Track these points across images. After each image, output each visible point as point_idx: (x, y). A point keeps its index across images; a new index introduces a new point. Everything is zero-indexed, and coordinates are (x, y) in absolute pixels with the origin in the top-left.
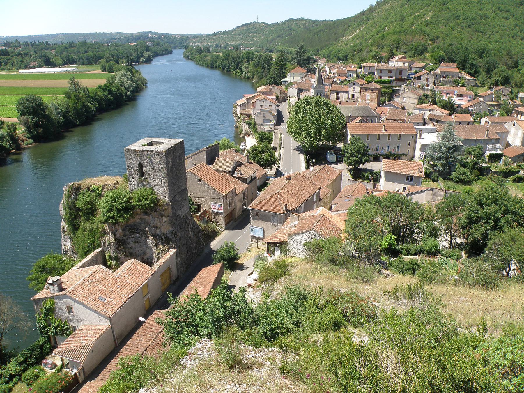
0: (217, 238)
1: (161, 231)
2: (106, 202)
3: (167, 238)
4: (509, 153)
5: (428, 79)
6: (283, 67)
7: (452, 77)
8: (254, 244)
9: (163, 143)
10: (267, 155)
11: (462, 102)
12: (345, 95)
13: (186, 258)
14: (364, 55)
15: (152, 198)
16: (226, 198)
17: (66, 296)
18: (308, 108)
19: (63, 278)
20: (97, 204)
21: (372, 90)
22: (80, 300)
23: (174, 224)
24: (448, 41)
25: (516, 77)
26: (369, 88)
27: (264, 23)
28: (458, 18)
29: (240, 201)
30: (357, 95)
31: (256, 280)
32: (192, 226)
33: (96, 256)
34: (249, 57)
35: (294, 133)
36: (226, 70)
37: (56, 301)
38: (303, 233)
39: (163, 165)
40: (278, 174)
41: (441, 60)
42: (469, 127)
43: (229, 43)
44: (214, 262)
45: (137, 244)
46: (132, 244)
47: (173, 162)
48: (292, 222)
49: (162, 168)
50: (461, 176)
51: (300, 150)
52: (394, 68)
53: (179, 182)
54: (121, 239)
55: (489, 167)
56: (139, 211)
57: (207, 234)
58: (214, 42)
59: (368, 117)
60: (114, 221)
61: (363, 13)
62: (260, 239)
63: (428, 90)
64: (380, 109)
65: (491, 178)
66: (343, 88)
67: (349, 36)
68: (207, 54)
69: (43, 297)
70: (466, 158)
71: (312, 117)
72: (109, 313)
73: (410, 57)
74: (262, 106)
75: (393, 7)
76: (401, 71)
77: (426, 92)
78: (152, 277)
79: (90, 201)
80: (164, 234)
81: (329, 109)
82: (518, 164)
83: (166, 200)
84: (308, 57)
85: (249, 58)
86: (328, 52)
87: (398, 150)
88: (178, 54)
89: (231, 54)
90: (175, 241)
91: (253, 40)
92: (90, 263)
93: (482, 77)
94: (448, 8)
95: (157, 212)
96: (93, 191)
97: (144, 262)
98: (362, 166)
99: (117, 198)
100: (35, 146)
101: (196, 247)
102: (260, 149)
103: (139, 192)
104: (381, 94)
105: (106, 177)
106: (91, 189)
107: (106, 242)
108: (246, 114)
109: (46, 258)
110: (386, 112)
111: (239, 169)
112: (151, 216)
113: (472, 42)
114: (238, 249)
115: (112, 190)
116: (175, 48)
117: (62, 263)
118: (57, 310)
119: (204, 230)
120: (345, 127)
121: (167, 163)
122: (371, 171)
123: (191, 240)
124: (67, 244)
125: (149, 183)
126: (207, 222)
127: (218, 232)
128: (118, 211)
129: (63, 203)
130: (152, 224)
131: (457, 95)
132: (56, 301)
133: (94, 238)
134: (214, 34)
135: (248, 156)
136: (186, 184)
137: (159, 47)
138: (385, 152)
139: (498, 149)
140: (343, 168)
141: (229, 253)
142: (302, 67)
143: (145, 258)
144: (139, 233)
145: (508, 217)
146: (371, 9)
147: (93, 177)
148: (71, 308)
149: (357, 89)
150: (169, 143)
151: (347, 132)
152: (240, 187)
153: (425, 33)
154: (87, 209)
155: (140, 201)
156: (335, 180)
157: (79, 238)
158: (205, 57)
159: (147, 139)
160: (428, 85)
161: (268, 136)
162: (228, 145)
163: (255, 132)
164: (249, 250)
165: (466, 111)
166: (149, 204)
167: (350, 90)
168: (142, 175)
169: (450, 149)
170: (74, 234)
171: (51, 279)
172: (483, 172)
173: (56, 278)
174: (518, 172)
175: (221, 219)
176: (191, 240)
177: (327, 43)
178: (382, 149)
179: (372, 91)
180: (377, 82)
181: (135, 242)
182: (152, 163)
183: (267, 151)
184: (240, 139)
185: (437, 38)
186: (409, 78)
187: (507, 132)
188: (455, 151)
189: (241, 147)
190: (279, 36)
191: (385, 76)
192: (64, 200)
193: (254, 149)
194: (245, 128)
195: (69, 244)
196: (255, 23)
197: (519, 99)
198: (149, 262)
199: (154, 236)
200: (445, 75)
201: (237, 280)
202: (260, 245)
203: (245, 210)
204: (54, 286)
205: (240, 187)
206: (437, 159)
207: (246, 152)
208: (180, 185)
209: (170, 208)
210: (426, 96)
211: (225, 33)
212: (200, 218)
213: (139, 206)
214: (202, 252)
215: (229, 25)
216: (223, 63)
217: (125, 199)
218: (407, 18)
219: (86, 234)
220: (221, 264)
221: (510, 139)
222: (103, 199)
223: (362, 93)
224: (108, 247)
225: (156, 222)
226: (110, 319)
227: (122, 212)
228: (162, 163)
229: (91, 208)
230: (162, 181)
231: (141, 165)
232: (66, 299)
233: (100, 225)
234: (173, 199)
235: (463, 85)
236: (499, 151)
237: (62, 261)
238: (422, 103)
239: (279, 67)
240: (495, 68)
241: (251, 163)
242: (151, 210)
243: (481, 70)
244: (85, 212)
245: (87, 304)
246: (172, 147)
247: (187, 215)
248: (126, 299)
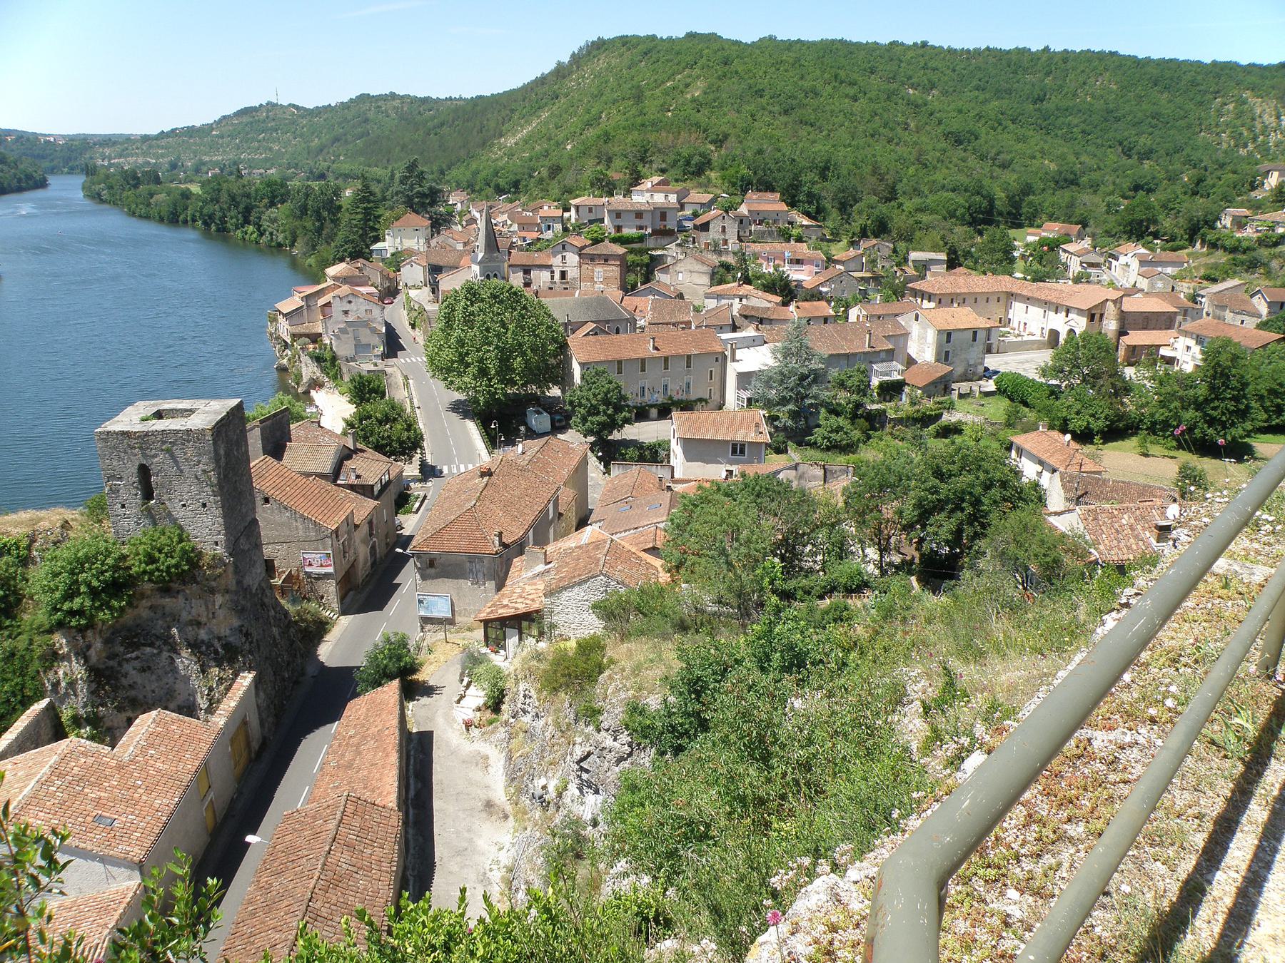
0: (327, 637)
1: (210, 632)
2: (56, 575)
3: (227, 646)
4: (918, 378)
5: (724, 228)
6: (369, 214)
7: (775, 221)
10: (399, 427)
11: (802, 276)
12: (545, 275)
13: (273, 693)
14: (569, 178)
15: (184, 552)
18: (475, 308)
21: (606, 259)
24: (752, 146)
25: (898, 221)
26: (600, 255)
27: (294, 106)
28: (760, 93)
29: (364, 541)
30: (572, 273)
31: (479, 709)
33: (36, 723)
34: (276, 194)
35: (445, 371)
36: (213, 228)
38: (580, 584)
39: (206, 464)
40: (428, 472)
41: (744, 186)
42: (829, 327)
43: (205, 158)
45: (147, 674)
47: (227, 455)
48: (531, 567)
49: (204, 472)
50: (833, 435)
51: (462, 409)
52: (646, 207)
55: (885, 411)
56: (148, 587)
58: (162, 156)
59: (607, 322)
60: (83, 622)
61: (541, 81)
63: (727, 252)
64: (631, 301)
65: (891, 434)
66: (538, 258)
67: (514, 135)
68: (153, 187)
70: (834, 397)
71: (488, 330)
72: (137, 853)
73: (677, 181)
74: (346, 312)
75: (609, 68)
76: (663, 214)
77: (723, 259)
78: (217, 745)
80: (219, 639)
81: (525, 308)
82: (937, 399)
83: (220, 550)
84: (430, 188)
85: (274, 197)
86: (468, 174)
87: (688, 392)
88: (67, 189)
89: (225, 186)
90: (250, 652)
91: (270, 149)
93: (834, 220)
94: (737, 72)
95: (198, 583)
98: (616, 436)
102: (378, 415)
104: (627, 268)
107: (58, 683)
108: (307, 335)
110: (644, 307)
111: (349, 464)
112: (180, 597)
113: (800, 145)
116: (52, 171)
120: (563, 347)
121: (217, 459)
122: (634, 443)
127: (327, 623)
128: (94, 593)
130: (185, 616)
131: (792, 262)
134: (162, 135)
137: (5, 168)
138: (660, 398)
139: (894, 372)
140: (575, 440)
141: (399, 658)
142: (417, 213)
144: (152, 645)
145: (995, 492)
146: (560, 72)
149: (572, 258)
150: (207, 413)
151: (568, 361)
152: (364, 508)
153: (698, 125)
155: (151, 560)
156: (577, 470)
158: (151, 195)
160: (726, 242)
161: (374, 385)
163: (335, 378)
165: (815, 295)
166: (177, 566)
167: (556, 261)
168: (148, 494)
169: (803, 378)
172: (875, 421)
174: (939, 416)
175: (330, 590)
177: (462, 153)
178: (653, 391)
179: (606, 260)
180: (614, 240)
181: (143, 670)
182: (176, 462)
183: (395, 419)
185: (726, 136)
186: (682, 229)
187: (906, 335)
188: (815, 381)
190: (336, 140)
191: (630, 227)
194: (309, 370)
196: (271, 106)
197: (910, 263)
199: (194, 646)
200: (759, 218)
201: (430, 719)
205: (364, 508)
206: (778, 404)
208: (244, 510)
209: (231, 569)
210: (727, 267)
211: (191, 131)
213: (151, 573)
214: (303, 674)
215: (203, 113)
216: (205, 211)
218: (648, 93)
221: (913, 350)
223: (584, 267)
225: (197, 609)
226: (140, 866)
228: (204, 459)
230: (204, 505)
231: (144, 471)
235: (799, 240)
236: (896, 377)
238: (720, 283)
239: (359, 216)
240: (856, 201)
243: (828, 206)
246: (222, 419)
248: (167, 811)
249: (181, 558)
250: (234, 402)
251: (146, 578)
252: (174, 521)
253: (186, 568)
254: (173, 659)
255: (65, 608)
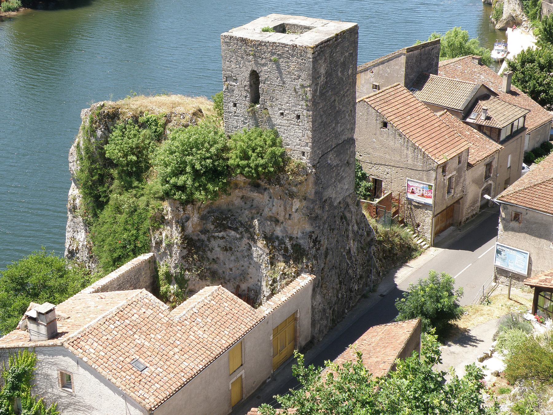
0: (412, 263)
1: (285, 230)
2: (172, 153)
3: (297, 248)
8: (502, 289)
9: (309, 28)
13: (334, 299)
15: (273, 154)
16: (444, 171)
17: (61, 350)
19: (61, 309)
20: (151, 155)
22: (90, 363)
23: (317, 217)
29: (476, 182)
31: (498, 375)
32: (356, 228)
33: (137, 270)
37: (40, 357)
39: (305, 79)
44: (399, 317)
45: (229, 254)
46: (218, 253)
47: (328, 74)
49: (302, 86)
53: (337, 123)
54: (195, 238)
57: (391, 250)
62: (518, 277)
69: (12, 345)
79: (137, 148)
80: (291, 238)
83: (305, 160)
90: (315, 257)
92: (121, 285)
95: (281, 185)
96: (143, 125)
97: (240, 296)
99: (197, 145)
100: (25, 16)
101: (361, 277)
102: (542, 61)
103: (244, 138)
105: (175, 98)
106: (141, 120)
107: (161, 242)
109: (29, 261)
111: (483, 104)
114: (461, 294)
115: (186, 126)
117: (61, 277)
118: (38, 378)
119: (384, 241)
121: (315, 76)
123: (350, 258)
124: (77, 236)
125: (269, 119)
126: (392, 222)
127: (416, 250)
128: (196, 174)
129: (78, 146)
130: (267, 212)
132: (40, 357)
133: (138, 230)
135: (510, 76)
136: (353, 129)
143: (244, 286)
144: (236, 230)
147: (147, 95)
148: (69, 378)
150: (324, 29)
152: (483, 149)
154: (127, 165)
155: (246, 157)
157: (106, 226)
159: (274, 16)
162: (461, 46)
163: (534, 18)
164: (487, 300)
166: (265, 166)
168: (255, 99)
170: (95, 215)
171: (35, 308)
173: (45, 307)
175: (427, 221)
176: (350, 258)
181: (226, 249)
182: (280, 73)
184: (493, 34)
189: (495, 55)
192: (80, 139)
193: (527, 59)
195: (81, 236)
198: (252, 298)
199: (269, 239)
202: (516, 292)
203: (486, 205)
204: (38, 324)
207: (505, 65)
208: (339, 129)
209: (312, 179)
212: (377, 212)
213: (243, 168)
214: (374, 291)
217: (213, 150)
219: (121, 218)
220: (414, 322)
222: (165, 145)
224: (165, 253)
225: (276, 208)
227: (203, 179)
228: (304, 75)
229: (137, 162)
230: (298, 117)
231: (255, 77)
232: (61, 357)
233: (153, 203)
234: (319, 162)
237: (62, 272)
241: (514, 94)
242: (269, 180)
244: (123, 171)
245: (104, 373)
246: (328, 40)
247: (349, 200)
249: (270, 160)
250: (356, 24)
251: (239, 171)
252: (272, 126)
253: (272, 169)
254: (250, 246)
255: (172, 181)
